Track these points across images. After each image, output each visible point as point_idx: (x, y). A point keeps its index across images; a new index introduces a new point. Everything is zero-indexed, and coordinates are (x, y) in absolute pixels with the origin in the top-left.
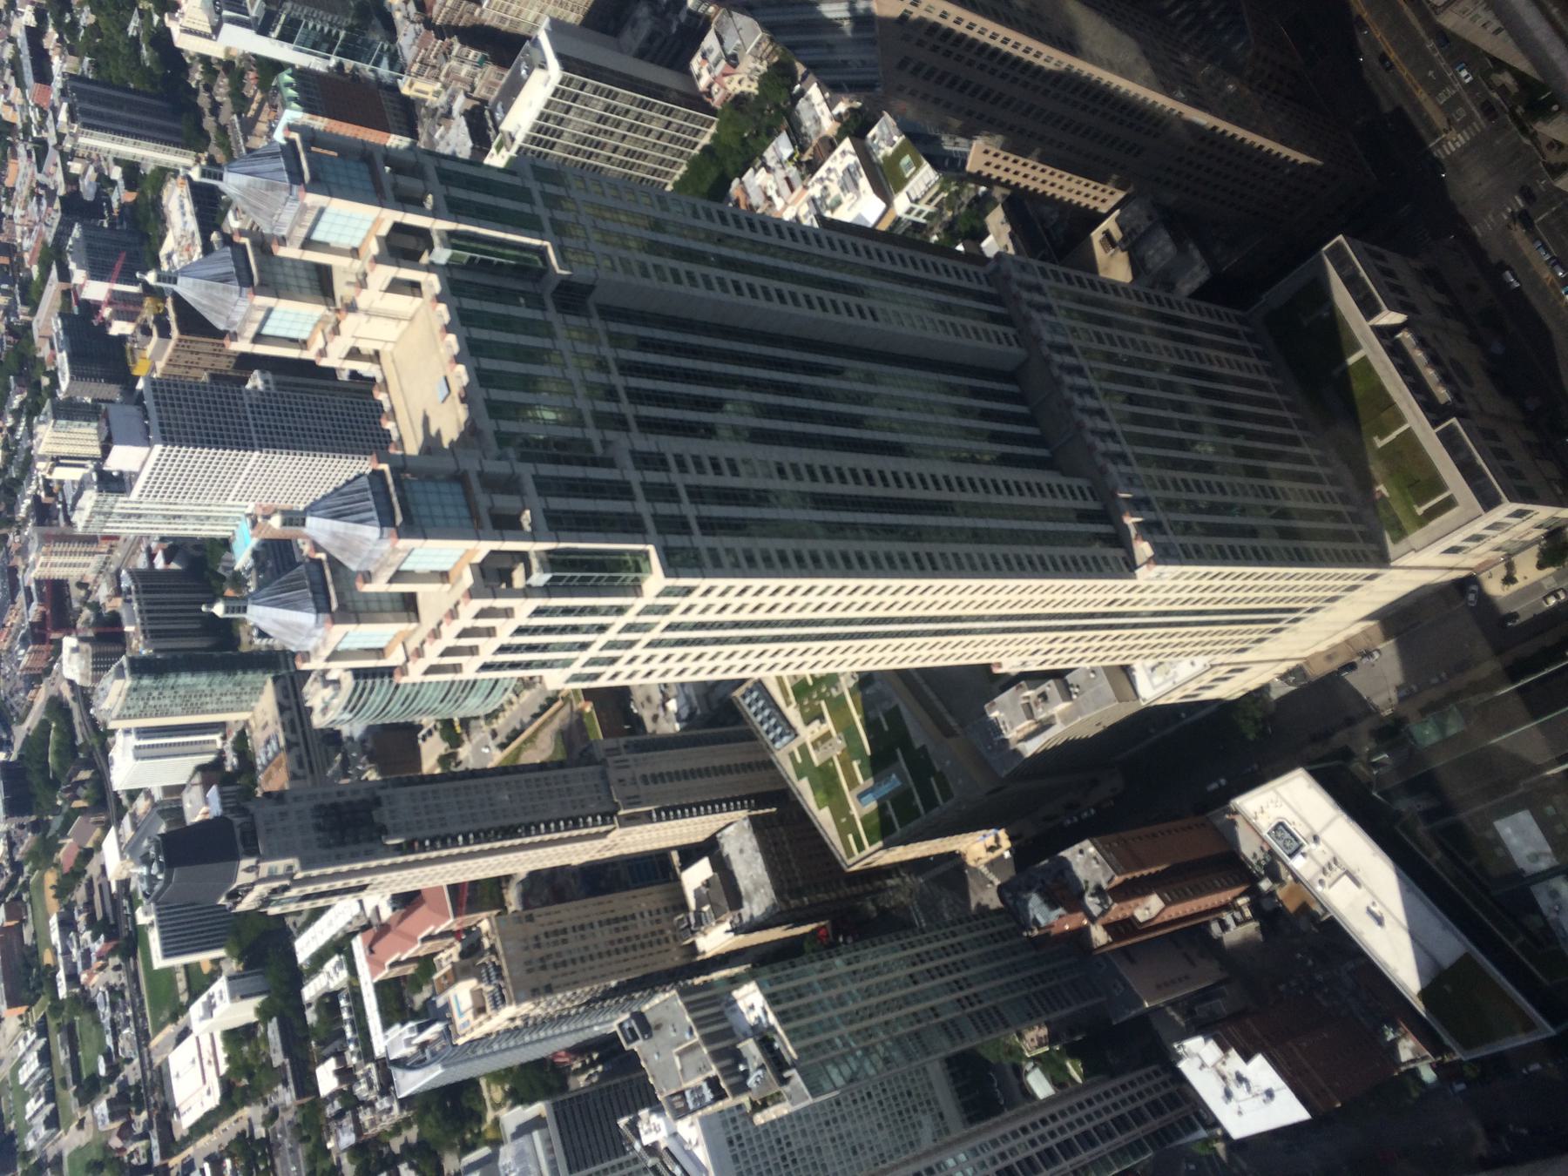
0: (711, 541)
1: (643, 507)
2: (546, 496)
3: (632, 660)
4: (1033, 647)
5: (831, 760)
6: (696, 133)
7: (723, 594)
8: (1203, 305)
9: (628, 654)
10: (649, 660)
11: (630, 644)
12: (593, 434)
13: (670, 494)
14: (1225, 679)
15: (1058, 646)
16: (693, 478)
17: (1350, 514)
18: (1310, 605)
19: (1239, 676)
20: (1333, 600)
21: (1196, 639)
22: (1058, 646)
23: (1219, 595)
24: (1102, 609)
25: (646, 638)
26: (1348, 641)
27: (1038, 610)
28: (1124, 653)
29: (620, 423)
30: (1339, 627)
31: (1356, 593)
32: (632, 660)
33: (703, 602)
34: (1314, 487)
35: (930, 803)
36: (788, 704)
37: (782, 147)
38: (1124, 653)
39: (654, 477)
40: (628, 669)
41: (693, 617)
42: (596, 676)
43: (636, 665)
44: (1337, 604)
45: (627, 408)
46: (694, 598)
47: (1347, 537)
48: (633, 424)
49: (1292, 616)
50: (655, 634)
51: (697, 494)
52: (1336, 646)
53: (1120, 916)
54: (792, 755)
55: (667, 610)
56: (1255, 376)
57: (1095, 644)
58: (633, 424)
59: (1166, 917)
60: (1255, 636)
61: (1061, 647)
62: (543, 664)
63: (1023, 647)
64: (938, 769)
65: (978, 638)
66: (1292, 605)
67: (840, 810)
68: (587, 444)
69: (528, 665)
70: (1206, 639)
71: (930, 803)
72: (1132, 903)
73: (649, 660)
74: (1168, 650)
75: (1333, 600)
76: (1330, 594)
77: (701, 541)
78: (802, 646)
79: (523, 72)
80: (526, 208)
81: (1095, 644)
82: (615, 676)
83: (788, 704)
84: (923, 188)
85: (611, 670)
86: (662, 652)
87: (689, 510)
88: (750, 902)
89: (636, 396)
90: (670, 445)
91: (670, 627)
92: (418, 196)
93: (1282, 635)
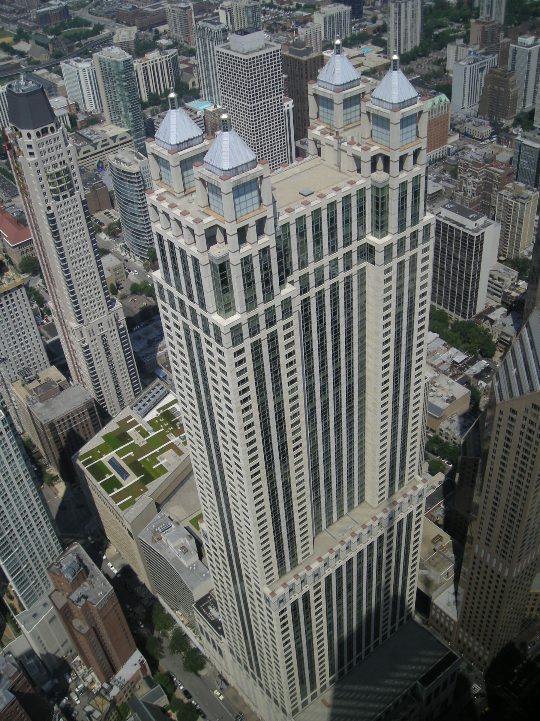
0: (395, 268)
1: (261, 309)
2: (242, 263)
3: (174, 316)
4: (216, 539)
5: (131, 439)
6: (458, 311)
7: (180, 380)
8: (414, 595)
9: (178, 314)
10: (177, 326)
11: (184, 314)
12: (296, 275)
13: (271, 323)
14: (214, 647)
15: (219, 552)
16: (281, 334)
17: (343, 670)
18: (263, 682)
19: (217, 654)
20: (268, 693)
21: (234, 626)
22: (219, 552)
23: (264, 651)
24: (244, 572)
25: (189, 322)
26: (245, 705)
27: (238, 538)
28: (224, 607)
29: (304, 289)
30: (253, 700)
31: (274, 704)
32: (174, 316)
33: (213, 350)
34: (389, 622)
35: (116, 498)
36: (158, 410)
37: (460, 357)
38: (224, 607)
39: (279, 312)
40: (169, 315)
41: (205, 346)
42: (163, 299)
43: (172, 319)
44: (266, 696)
45: (312, 293)
46: (215, 345)
47: (341, 664)
48: (305, 296)
49: (255, 674)
50: (192, 327)
51: (273, 338)
52: (242, 699)
53: (74, 611)
54: (130, 417)
55: (207, 332)
56: (381, 630)
57: (223, 573)
58: (305, 296)
59: (78, 636)
60: (241, 657)
61: (224, 581)
62: (166, 268)
63: (215, 533)
64: (136, 499)
65: (215, 502)
66: (262, 673)
67: (103, 449)
68: (289, 272)
69: (164, 260)
70: (236, 632)
71: (116, 498)
72: (82, 616)
73: (177, 326)
74: (226, 613)
75: (268, 693)
76: (271, 691)
77: (247, 344)
78: (204, 448)
79: (471, 216)
80: (408, 223)
81: (223, 573)
82: (164, 308)
83: (158, 410)
84: (74, 347)
85: (167, 306)
86: (182, 333)
87: (263, 334)
88: (47, 406)
89: (320, 296)
90: (295, 318)
91: (197, 335)
92: (404, 167)
93: (245, 672)
